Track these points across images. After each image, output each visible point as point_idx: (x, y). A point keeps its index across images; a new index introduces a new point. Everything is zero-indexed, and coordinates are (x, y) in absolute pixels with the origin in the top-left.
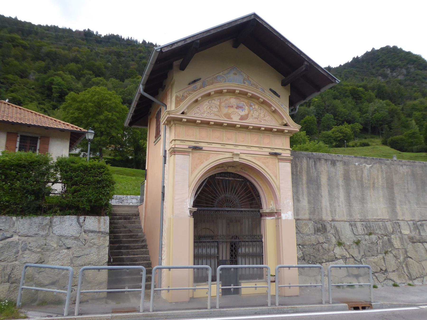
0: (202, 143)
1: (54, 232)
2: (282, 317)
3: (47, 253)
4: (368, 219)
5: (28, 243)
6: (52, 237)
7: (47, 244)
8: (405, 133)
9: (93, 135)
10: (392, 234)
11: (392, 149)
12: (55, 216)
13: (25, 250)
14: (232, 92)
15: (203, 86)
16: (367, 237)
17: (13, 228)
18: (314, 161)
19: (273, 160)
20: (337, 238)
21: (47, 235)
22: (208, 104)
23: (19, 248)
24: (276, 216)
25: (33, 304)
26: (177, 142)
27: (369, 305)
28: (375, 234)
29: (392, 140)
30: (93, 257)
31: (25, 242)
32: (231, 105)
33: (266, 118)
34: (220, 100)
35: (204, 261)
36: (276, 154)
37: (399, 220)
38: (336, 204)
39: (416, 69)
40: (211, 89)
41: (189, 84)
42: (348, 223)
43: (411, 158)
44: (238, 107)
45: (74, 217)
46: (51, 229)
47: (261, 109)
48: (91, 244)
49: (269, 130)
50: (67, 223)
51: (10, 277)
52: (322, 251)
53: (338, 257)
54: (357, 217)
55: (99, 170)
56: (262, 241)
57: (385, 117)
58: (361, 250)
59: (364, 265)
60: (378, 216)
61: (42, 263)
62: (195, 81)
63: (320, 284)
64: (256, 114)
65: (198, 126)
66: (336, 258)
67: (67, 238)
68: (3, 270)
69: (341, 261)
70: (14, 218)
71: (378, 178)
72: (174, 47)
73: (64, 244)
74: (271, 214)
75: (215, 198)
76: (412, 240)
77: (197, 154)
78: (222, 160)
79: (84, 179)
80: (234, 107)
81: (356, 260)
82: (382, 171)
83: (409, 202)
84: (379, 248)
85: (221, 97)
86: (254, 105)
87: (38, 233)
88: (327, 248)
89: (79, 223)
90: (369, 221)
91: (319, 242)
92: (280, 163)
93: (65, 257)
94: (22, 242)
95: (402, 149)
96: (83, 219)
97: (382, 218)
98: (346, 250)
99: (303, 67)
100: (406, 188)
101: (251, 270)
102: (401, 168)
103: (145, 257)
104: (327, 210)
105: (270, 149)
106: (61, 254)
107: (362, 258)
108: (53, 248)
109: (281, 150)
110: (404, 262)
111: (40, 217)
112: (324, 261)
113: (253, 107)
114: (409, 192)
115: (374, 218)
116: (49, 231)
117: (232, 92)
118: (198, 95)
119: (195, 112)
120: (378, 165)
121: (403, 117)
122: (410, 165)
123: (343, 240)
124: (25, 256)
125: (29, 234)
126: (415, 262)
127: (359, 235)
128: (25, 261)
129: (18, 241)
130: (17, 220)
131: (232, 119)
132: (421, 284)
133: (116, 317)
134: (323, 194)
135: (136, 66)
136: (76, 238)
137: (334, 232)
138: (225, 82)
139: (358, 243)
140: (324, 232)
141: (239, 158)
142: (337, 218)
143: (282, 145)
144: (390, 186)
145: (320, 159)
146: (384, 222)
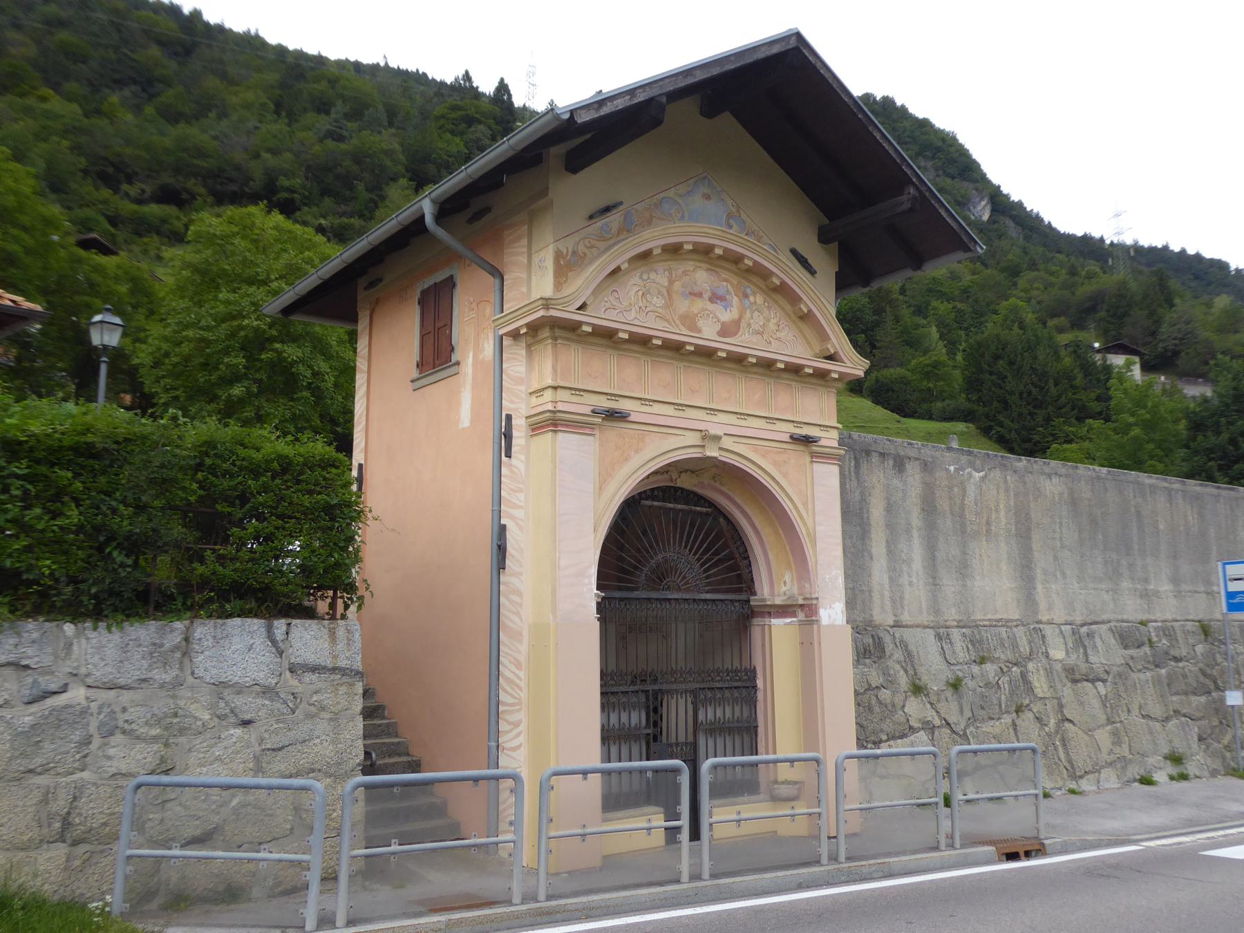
0: (628, 401)
1: (200, 672)
2: (790, 902)
3: (182, 740)
4: (975, 621)
5: (118, 709)
6: (192, 688)
7: (181, 712)
8: (914, 362)
9: (119, 332)
10: (1030, 660)
11: (878, 407)
12: (197, 622)
13: (112, 734)
14: (704, 252)
15: (627, 229)
16: (976, 669)
17: (68, 662)
18: (855, 458)
19: (798, 456)
20: (911, 672)
21: (177, 684)
22: (640, 282)
23: (93, 729)
24: (801, 616)
25: (146, 908)
26: (563, 395)
27: (1037, 847)
28: (993, 660)
29: (877, 380)
30: (322, 749)
31: (109, 705)
32: (696, 290)
33: (781, 335)
34: (671, 274)
35: (635, 749)
36: (807, 441)
37: (1040, 622)
38: (904, 580)
39: (941, 172)
40: (653, 238)
41: (591, 217)
42: (931, 632)
43: (928, 437)
44: (715, 298)
45: (256, 624)
46: (186, 661)
47: (769, 308)
48: (312, 708)
49: (794, 370)
50: (238, 643)
51: (66, 823)
52: (877, 709)
53: (916, 725)
54: (951, 614)
55: (324, 473)
56: (755, 687)
57: (858, 310)
58: (964, 705)
59: (974, 747)
60: (996, 612)
61: (166, 772)
62: (607, 209)
63: (510, 837)
64: (757, 321)
65: (614, 348)
66: (911, 727)
67: (239, 689)
68: (45, 801)
69: (922, 735)
70: (69, 628)
71: (997, 511)
72: (605, 110)
73: (232, 711)
74: (784, 610)
75: (639, 562)
76: (1074, 676)
77: (614, 432)
78: (671, 455)
79: (282, 499)
80: (706, 296)
81: (954, 732)
82: (1007, 490)
83: (1064, 575)
84: (1003, 697)
85: (674, 264)
86: (754, 294)
87: (149, 675)
88: (888, 701)
89: (274, 642)
90: (977, 626)
91: (870, 685)
92: (815, 465)
93: (238, 752)
94: (101, 708)
95: (903, 409)
96: (284, 628)
97: (1004, 616)
98: (931, 704)
99: (905, 201)
100: (1057, 536)
101: (625, 776)
102: (1048, 482)
103: (393, 744)
104: (882, 596)
105: (791, 425)
106: (225, 743)
107: (967, 726)
108: (199, 723)
109: (817, 428)
110: (1057, 732)
111: (153, 625)
112: (884, 737)
113: (752, 299)
114: (1063, 547)
115: (990, 616)
116: (181, 669)
117: (704, 252)
118: (621, 255)
119: (608, 305)
120: (997, 474)
121: (905, 312)
122: (1067, 476)
123: (925, 679)
124: (111, 752)
125: (122, 681)
126: (1080, 732)
127: (958, 663)
128: (113, 770)
129: (84, 703)
130: (78, 634)
131: (699, 331)
132: (1094, 788)
133: (460, 922)
134: (874, 551)
135: (32, 51)
136: (268, 691)
137: (902, 658)
138: (682, 218)
139: (956, 685)
140: (880, 658)
141: (721, 449)
142: (906, 618)
143: (819, 412)
144: (1023, 532)
145: (868, 453)
146: (1010, 627)
